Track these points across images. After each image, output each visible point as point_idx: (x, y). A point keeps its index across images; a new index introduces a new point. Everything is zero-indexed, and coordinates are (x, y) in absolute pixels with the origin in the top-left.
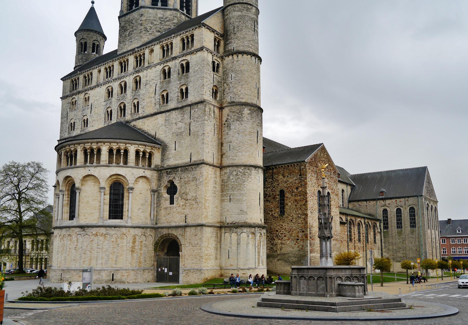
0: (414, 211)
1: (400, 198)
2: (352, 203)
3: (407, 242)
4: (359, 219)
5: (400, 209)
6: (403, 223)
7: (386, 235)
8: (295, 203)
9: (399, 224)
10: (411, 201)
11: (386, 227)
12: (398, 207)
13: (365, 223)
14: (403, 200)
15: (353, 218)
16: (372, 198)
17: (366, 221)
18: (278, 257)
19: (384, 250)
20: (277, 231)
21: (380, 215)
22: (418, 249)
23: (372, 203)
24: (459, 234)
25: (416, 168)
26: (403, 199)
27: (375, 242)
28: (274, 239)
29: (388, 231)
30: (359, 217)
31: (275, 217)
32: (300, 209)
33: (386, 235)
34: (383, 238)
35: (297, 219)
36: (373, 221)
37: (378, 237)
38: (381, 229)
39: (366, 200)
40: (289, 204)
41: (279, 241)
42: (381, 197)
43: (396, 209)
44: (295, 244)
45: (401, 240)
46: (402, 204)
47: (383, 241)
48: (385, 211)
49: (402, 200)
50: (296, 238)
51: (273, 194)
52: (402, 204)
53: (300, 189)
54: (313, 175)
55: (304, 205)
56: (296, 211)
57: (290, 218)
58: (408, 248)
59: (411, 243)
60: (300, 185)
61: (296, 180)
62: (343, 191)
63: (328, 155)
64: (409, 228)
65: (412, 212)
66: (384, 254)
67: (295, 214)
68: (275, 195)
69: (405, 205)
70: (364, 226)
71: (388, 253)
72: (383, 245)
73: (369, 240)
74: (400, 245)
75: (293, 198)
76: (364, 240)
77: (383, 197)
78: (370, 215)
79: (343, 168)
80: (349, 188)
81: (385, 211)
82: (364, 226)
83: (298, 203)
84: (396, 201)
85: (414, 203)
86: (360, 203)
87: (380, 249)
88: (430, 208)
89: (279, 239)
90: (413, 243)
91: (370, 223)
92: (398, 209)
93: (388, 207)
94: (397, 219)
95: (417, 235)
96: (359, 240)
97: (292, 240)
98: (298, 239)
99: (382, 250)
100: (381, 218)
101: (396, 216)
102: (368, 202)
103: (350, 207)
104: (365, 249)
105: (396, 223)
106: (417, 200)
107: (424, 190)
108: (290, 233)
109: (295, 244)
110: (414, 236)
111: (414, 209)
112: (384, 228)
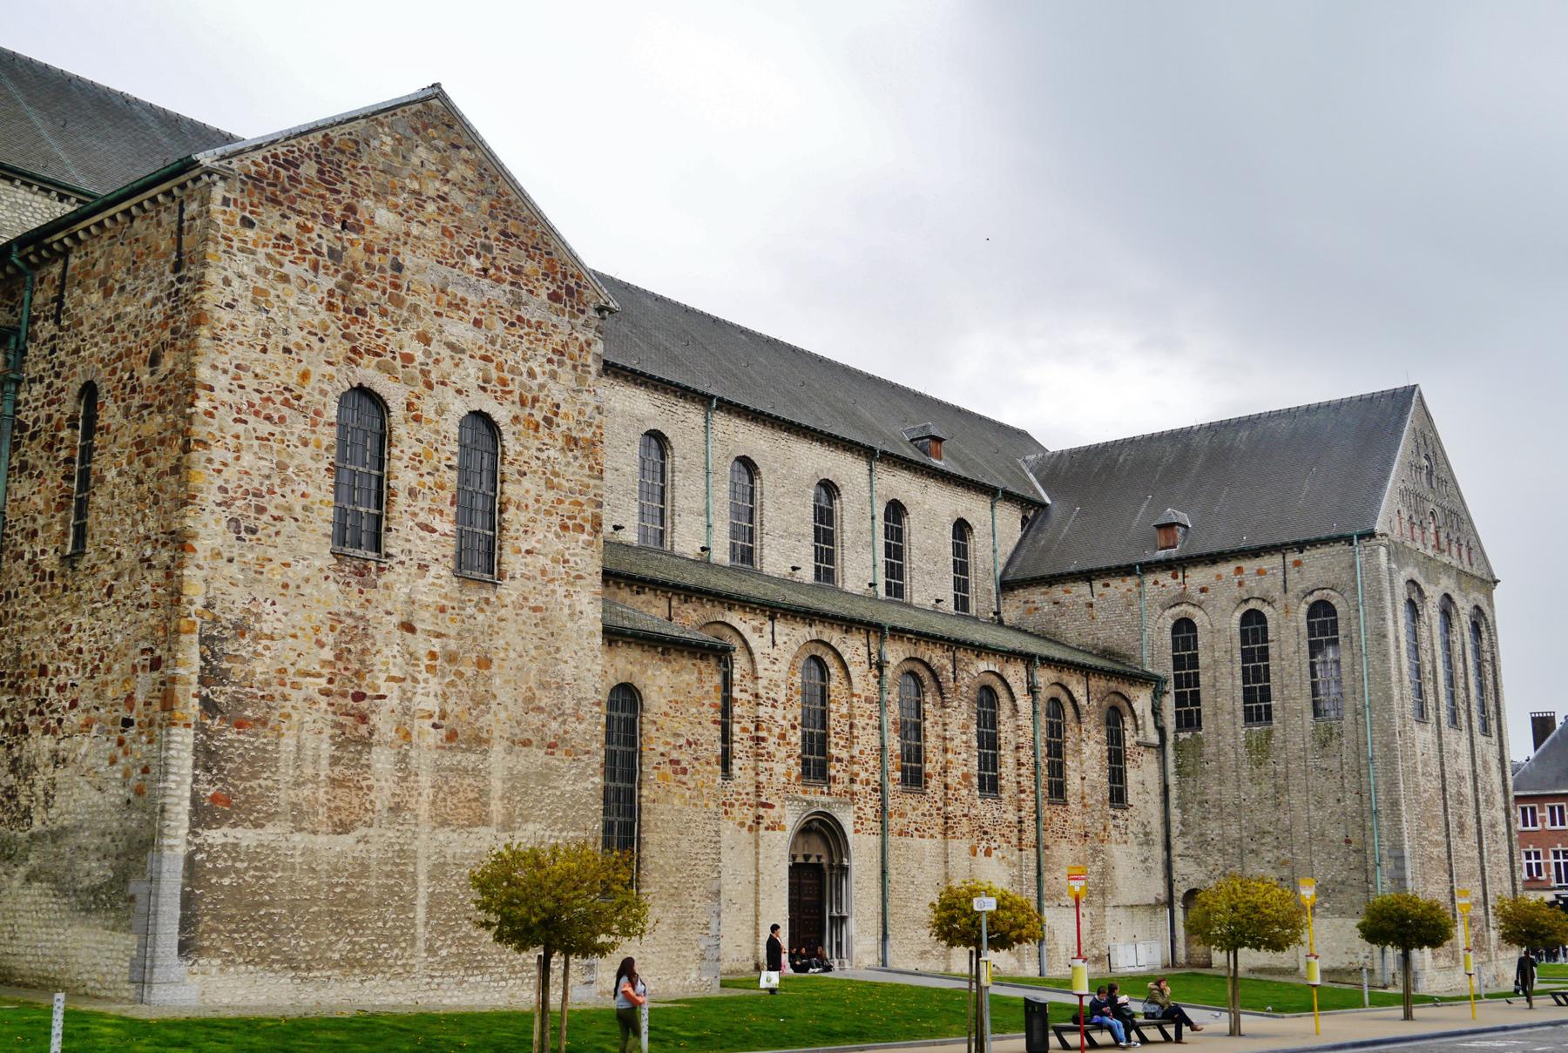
0: (1335, 623)
1: (1256, 553)
3: (1296, 798)
4: (983, 665)
6: (1275, 693)
7: (1189, 761)
10: (1318, 567)
11: (1189, 720)
12: (1252, 605)
13: (1032, 690)
14: (1271, 562)
15: (938, 657)
16: (1114, 563)
17: (1044, 677)
18: (33, 860)
19: (1178, 846)
21: (1158, 657)
22: (1356, 838)
25: (1361, 399)
26: (1277, 560)
27: (1118, 797)
29: (1199, 739)
30: (981, 650)
33: (1189, 761)
34: (1172, 780)
36: (1098, 684)
37: (1142, 774)
38: (1161, 731)
39: (1087, 576)
40: (111, 474)
42: (1161, 554)
43: (1238, 615)
44: (113, 762)
46: (1271, 584)
47: (1173, 793)
48: (1184, 630)
50: (123, 713)
52: (1271, 584)
53: (167, 362)
55: (175, 470)
56: (134, 524)
58: (1301, 832)
59: (1320, 804)
60: (167, 335)
62: (962, 528)
63: (491, 172)
66: (1179, 866)
69: (1285, 591)
70: (1024, 703)
71: (1198, 861)
73: (1073, 783)
74: (1263, 817)
76: (1027, 783)
77: (1174, 553)
78: (1106, 653)
79: (1022, 435)
80: (1009, 521)
81: (1184, 630)
82: (1024, 703)
84: (1239, 570)
85: (1331, 578)
86: (1058, 592)
87: (1158, 837)
90: (1331, 801)
91: (1079, 692)
93: (1198, 605)
95: (1347, 754)
96: (989, 785)
98: (127, 723)
99: (1168, 847)
100: (1166, 669)
101: (1238, 656)
102: (1098, 585)
103: (1011, 614)
104: (1030, 836)
105: (1240, 694)
106: (1346, 560)
109: (113, 762)
110: (1334, 764)
112: (1180, 727)
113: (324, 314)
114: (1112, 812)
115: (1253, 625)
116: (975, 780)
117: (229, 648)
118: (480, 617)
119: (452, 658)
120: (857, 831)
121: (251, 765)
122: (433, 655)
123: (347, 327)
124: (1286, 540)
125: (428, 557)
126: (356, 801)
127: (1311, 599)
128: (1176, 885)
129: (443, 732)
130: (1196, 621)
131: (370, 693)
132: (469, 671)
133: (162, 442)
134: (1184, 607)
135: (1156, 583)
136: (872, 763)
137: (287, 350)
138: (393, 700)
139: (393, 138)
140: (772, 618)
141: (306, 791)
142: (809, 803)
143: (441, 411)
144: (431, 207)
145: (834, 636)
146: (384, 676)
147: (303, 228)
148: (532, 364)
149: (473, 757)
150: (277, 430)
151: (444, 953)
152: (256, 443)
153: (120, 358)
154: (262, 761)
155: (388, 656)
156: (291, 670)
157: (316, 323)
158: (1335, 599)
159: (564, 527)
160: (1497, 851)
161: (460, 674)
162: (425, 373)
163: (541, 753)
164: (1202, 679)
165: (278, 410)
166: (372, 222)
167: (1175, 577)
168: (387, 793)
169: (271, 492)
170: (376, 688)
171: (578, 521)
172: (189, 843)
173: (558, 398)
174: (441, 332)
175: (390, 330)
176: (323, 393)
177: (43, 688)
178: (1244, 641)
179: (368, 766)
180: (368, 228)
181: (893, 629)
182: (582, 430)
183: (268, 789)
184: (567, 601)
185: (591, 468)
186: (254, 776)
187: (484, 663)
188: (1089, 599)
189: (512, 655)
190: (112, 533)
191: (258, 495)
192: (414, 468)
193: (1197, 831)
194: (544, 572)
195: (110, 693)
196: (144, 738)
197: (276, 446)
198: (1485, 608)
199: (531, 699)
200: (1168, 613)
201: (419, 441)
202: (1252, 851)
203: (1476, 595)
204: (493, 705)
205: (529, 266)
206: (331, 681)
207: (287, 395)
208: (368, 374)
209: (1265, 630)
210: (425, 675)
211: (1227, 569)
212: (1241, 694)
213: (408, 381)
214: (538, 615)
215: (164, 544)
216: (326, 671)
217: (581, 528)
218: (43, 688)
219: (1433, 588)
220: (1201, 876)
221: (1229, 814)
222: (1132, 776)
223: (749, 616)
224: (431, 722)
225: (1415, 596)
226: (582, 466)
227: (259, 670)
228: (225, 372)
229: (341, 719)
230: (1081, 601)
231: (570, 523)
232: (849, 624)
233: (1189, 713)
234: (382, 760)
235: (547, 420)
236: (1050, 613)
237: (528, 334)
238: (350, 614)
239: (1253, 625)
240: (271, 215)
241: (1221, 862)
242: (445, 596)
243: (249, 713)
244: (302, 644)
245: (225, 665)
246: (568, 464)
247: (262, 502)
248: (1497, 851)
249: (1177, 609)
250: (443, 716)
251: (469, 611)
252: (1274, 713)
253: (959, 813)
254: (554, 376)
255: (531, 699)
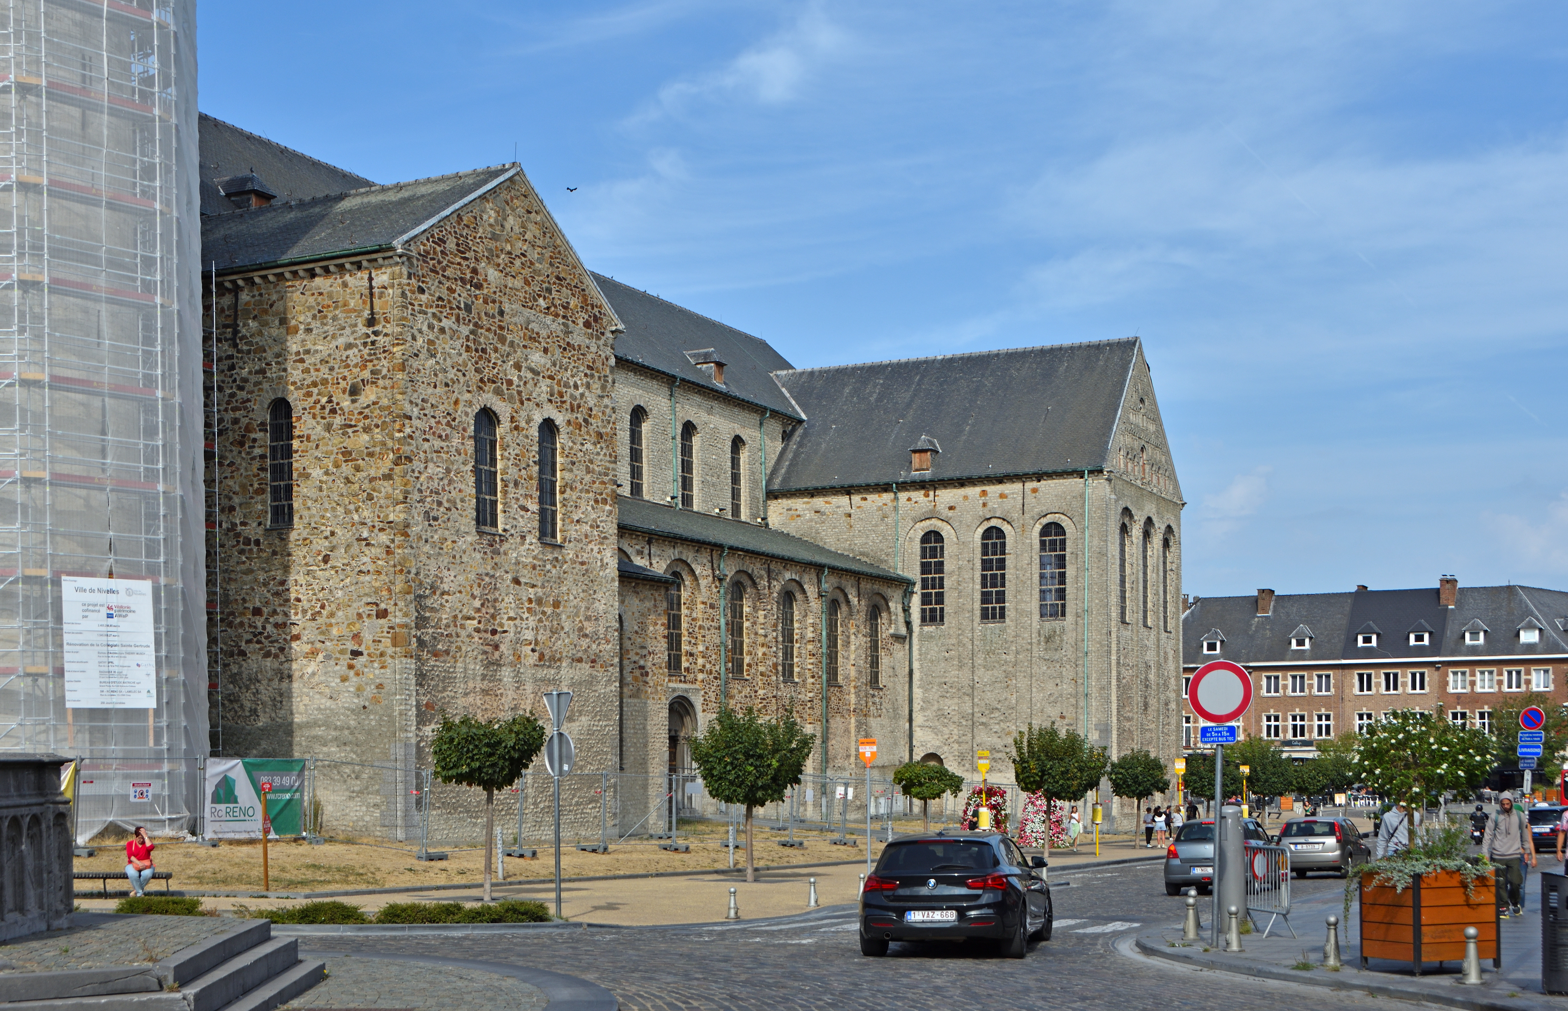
0: (1063, 542)
2: (785, 503)
5: (1000, 533)
6: (1009, 596)
8: (347, 469)
9: (993, 606)
12: (994, 523)
14: (1013, 488)
15: (757, 568)
16: (872, 480)
18: (264, 744)
19: (918, 718)
20: (257, 612)
23: (876, 500)
24: (1300, 655)
26: (1018, 486)
28: (243, 653)
31: (247, 541)
32: (370, 498)
34: (916, 665)
35: (355, 549)
36: (865, 586)
39: (848, 490)
40: (316, 473)
41: (269, 662)
44: (344, 679)
45: (998, 673)
47: (916, 676)
48: (932, 539)
49: (1008, 488)
50: (351, 646)
51: (236, 421)
53: (369, 395)
54: (445, 323)
56: (347, 512)
57: (320, 544)
60: (366, 374)
61: (349, 346)
64: (1036, 617)
65: (1053, 545)
66: (918, 733)
67: (342, 525)
68: (248, 429)
72: (917, 692)
75: (335, 442)
81: (932, 539)
83: (358, 469)
84: (984, 493)
86: (819, 502)
88: (1136, 532)
89: (268, 655)
92: (988, 533)
94: (984, 577)
97: (328, 657)
98: (356, 654)
99: (911, 720)
100: (914, 573)
101: (978, 565)
102: (856, 498)
105: (978, 596)
107: (1118, 439)
108: (320, 620)
109: (344, 679)
111: (1064, 533)
113: (465, 355)
114: (871, 692)
115: (994, 539)
116: (780, 668)
117: (429, 602)
118: (554, 571)
119: (539, 602)
120: (704, 711)
121: (443, 681)
122: (530, 601)
123: (477, 363)
124: (1027, 470)
125: (525, 529)
126: (495, 704)
127: (1045, 521)
128: (915, 749)
129: (537, 654)
130: (943, 534)
131: (499, 629)
132: (549, 610)
133: (371, 455)
134: (934, 521)
135: (909, 499)
136: (714, 657)
137: (447, 385)
138: (511, 635)
139: (496, 211)
140: (649, 543)
141: (470, 699)
142: (674, 690)
143: (529, 421)
144: (518, 263)
145: (689, 555)
146: (506, 617)
147: (451, 290)
148: (576, 379)
149: (553, 672)
150: (444, 444)
151: (542, 805)
152: (435, 455)
153: (314, 384)
154: (448, 679)
155: (508, 604)
156: (460, 616)
157: (460, 362)
158: (1065, 523)
159: (596, 501)
160: (1168, 724)
161: (544, 613)
162: (519, 393)
163: (588, 666)
164: (946, 583)
165: (444, 430)
166: (486, 280)
167: (927, 496)
168: (510, 698)
169: (444, 490)
170: (501, 625)
171: (604, 496)
172: (417, 735)
173: (591, 404)
174: (526, 360)
175: (499, 362)
176: (467, 414)
177: (259, 624)
178: (985, 552)
179: (500, 680)
180: (485, 285)
181: (731, 548)
182: (605, 427)
183: (453, 698)
184: (599, 557)
185: (610, 455)
186: (444, 689)
187: (556, 604)
188: (848, 509)
189: (571, 597)
190: (323, 517)
191: (437, 493)
192: (517, 465)
193: (935, 708)
194: (586, 536)
195: (335, 631)
196: (376, 665)
197: (444, 456)
198: (1174, 526)
199: (581, 629)
200: (918, 525)
201: (518, 444)
202: (983, 724)
203: (1169, 516)
204: (562, 634)
205: (573, 302)
206: (479, 622)
207: (449, 418)
208: (489, 399)
209: (1003, 545)
210: (526, 615)
211: (973, 491)
212: (979, 597)
213: (511, 399)
214: (585, 567)
215: (382, 530)
216: (477, 615)
217: (605, 501)
218: (259, 624)
219: (1140, 513)
220: (938, 743)
221: (964, 694)
222: (885, 661)
223: (634, 542)
224: (530, 647)
225: (1127, 520)
226: (605, 454)
227: (444, 616)
228: (417, 405)
229: (486, 648)
230: (840, 511)
231: (599, 498)
232: (699, 544)
233: (933, 611)
234: (506, 674)
235: (585, 420)
236: (811, 520)
237: (573, 356)
238: (487, 574)
239: (994, 539)
240: (432, 283)
241: (956, 731)
242: (535, 558)
243: (440, 647)
244: (465, 598)
245: (428, 614)
246: (598, 454)
247: (440, 498)
248: (1168, 724)
249: (928, 522)
250: (537, 643)
251: (548, 567)
252: (1007, 613)
253: (770, 695)
254: (588, 386)
255: (581, 629)
